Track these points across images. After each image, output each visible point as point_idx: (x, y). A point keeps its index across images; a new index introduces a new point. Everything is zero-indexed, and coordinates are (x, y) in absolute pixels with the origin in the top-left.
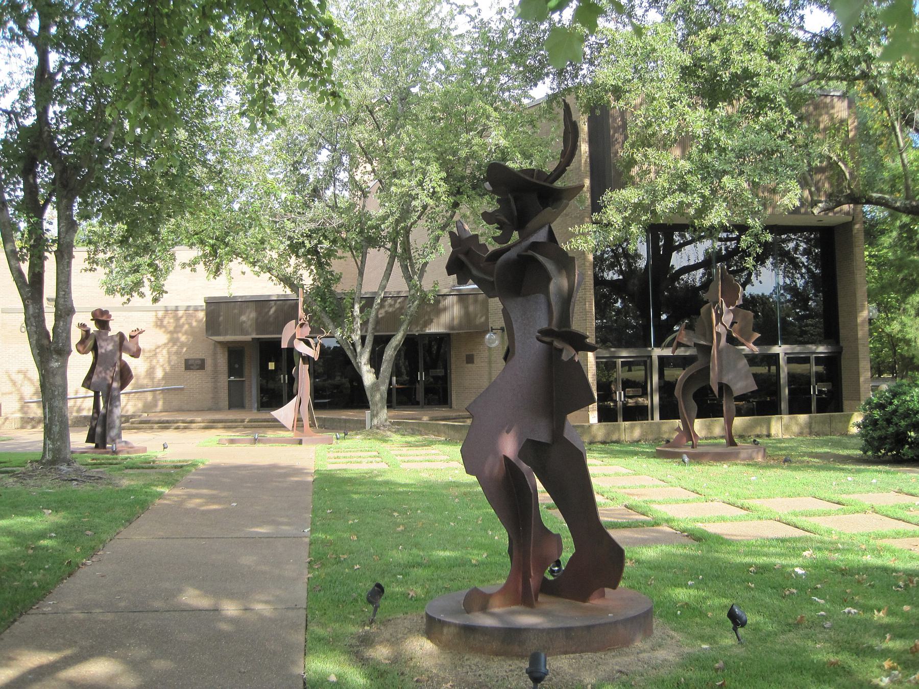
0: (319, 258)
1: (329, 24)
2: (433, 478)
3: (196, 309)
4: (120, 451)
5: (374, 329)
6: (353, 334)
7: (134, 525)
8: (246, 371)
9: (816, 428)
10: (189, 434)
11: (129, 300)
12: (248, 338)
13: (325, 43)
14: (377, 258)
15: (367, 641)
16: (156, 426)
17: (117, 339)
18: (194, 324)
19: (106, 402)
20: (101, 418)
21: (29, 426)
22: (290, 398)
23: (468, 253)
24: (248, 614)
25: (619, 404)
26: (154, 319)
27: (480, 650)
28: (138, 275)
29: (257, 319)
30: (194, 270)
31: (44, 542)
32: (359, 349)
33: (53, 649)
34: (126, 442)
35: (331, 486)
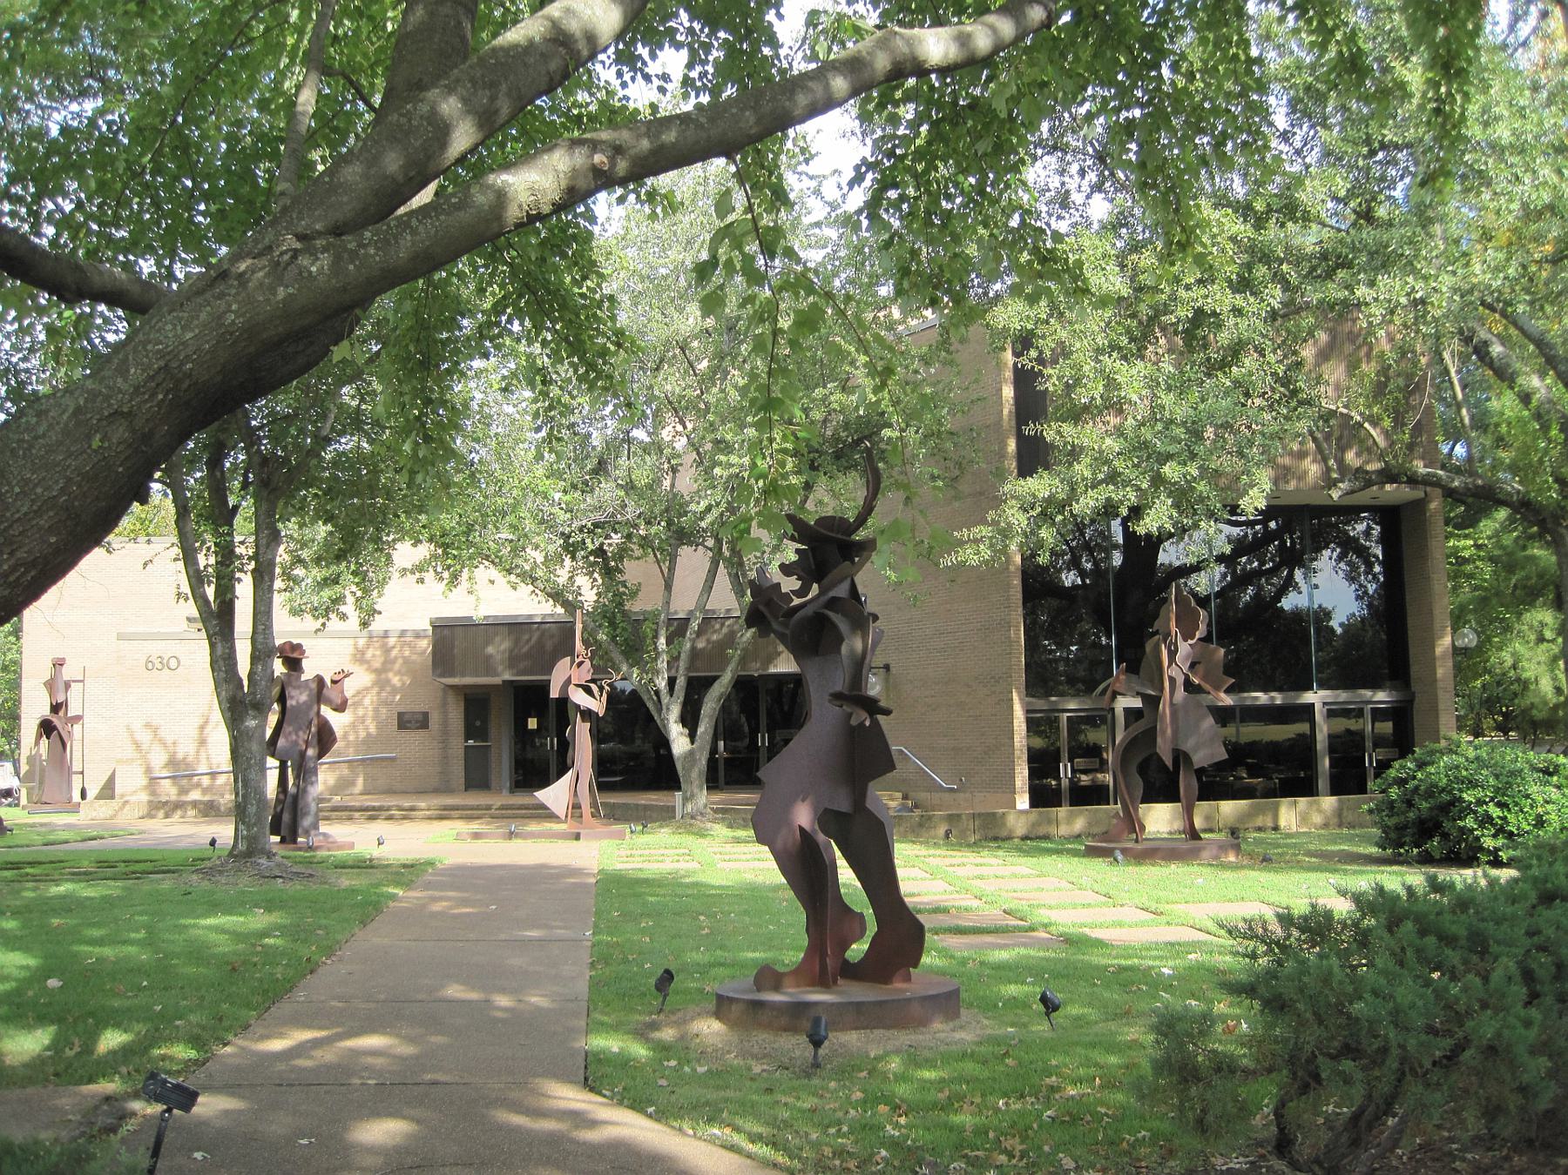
0: (606, 560)
1: (620, 333)
2: (760, 879)
3: (418, 635)
4: (318, 848)
5: (688, 669)
6: (658, 677)
7: (369, 927)
8: (493, 731)
9: (1349, 816)
10: (408, 826)
11: (324, 625)
12: (497, 680)
13: (616, 353)
14: (693, 562)
15: (654, 1026)
16: (357, 814)
17: (314, 686)
19: (297, 777)
20: (289, 800)
21: (161, 814)
22: (563, 769)
23: (769, 603)
24: (522, 1006)
25: (1065, 783)
26: (351, 650)
27: (768, 1027)
28: (338, 588)
29: (511, 651)
30: (421, 581)
31: (269, 941)
32: (665, 699)
33: (321, 1028)
34: (324, 835)
35: (617, 886)
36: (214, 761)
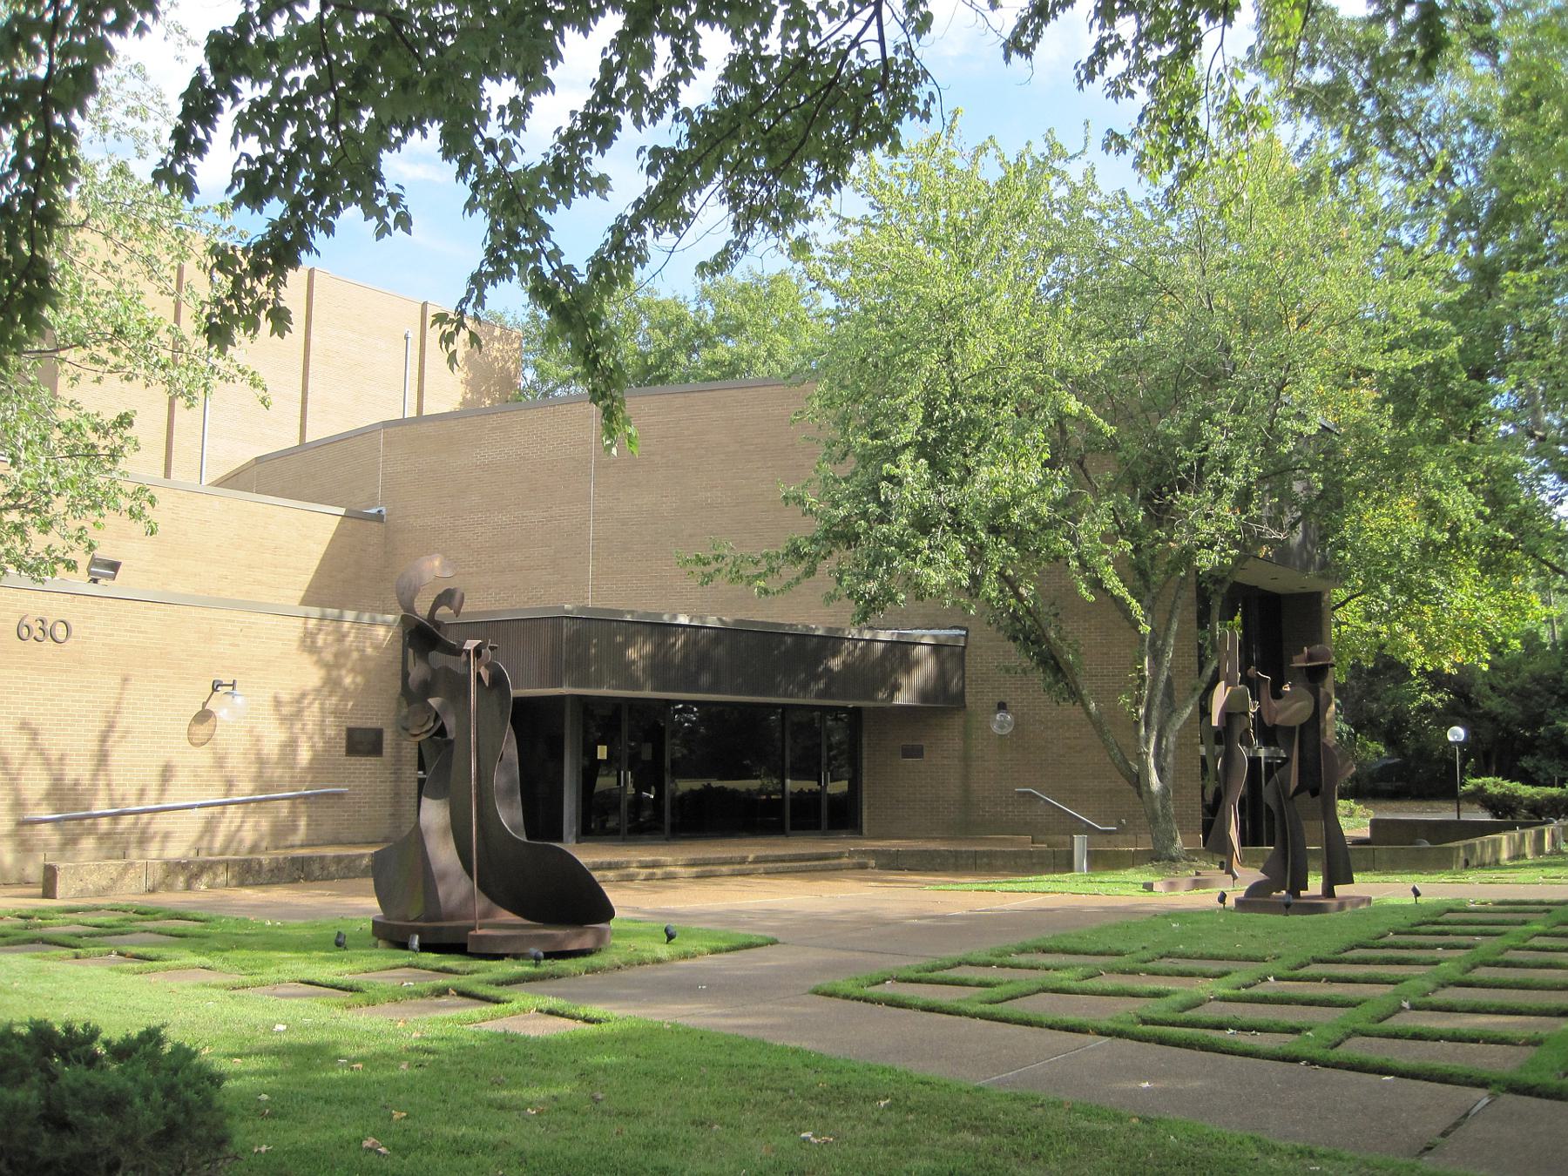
18: (369, 651)
26: (299, 633)
36: (117, 795)
